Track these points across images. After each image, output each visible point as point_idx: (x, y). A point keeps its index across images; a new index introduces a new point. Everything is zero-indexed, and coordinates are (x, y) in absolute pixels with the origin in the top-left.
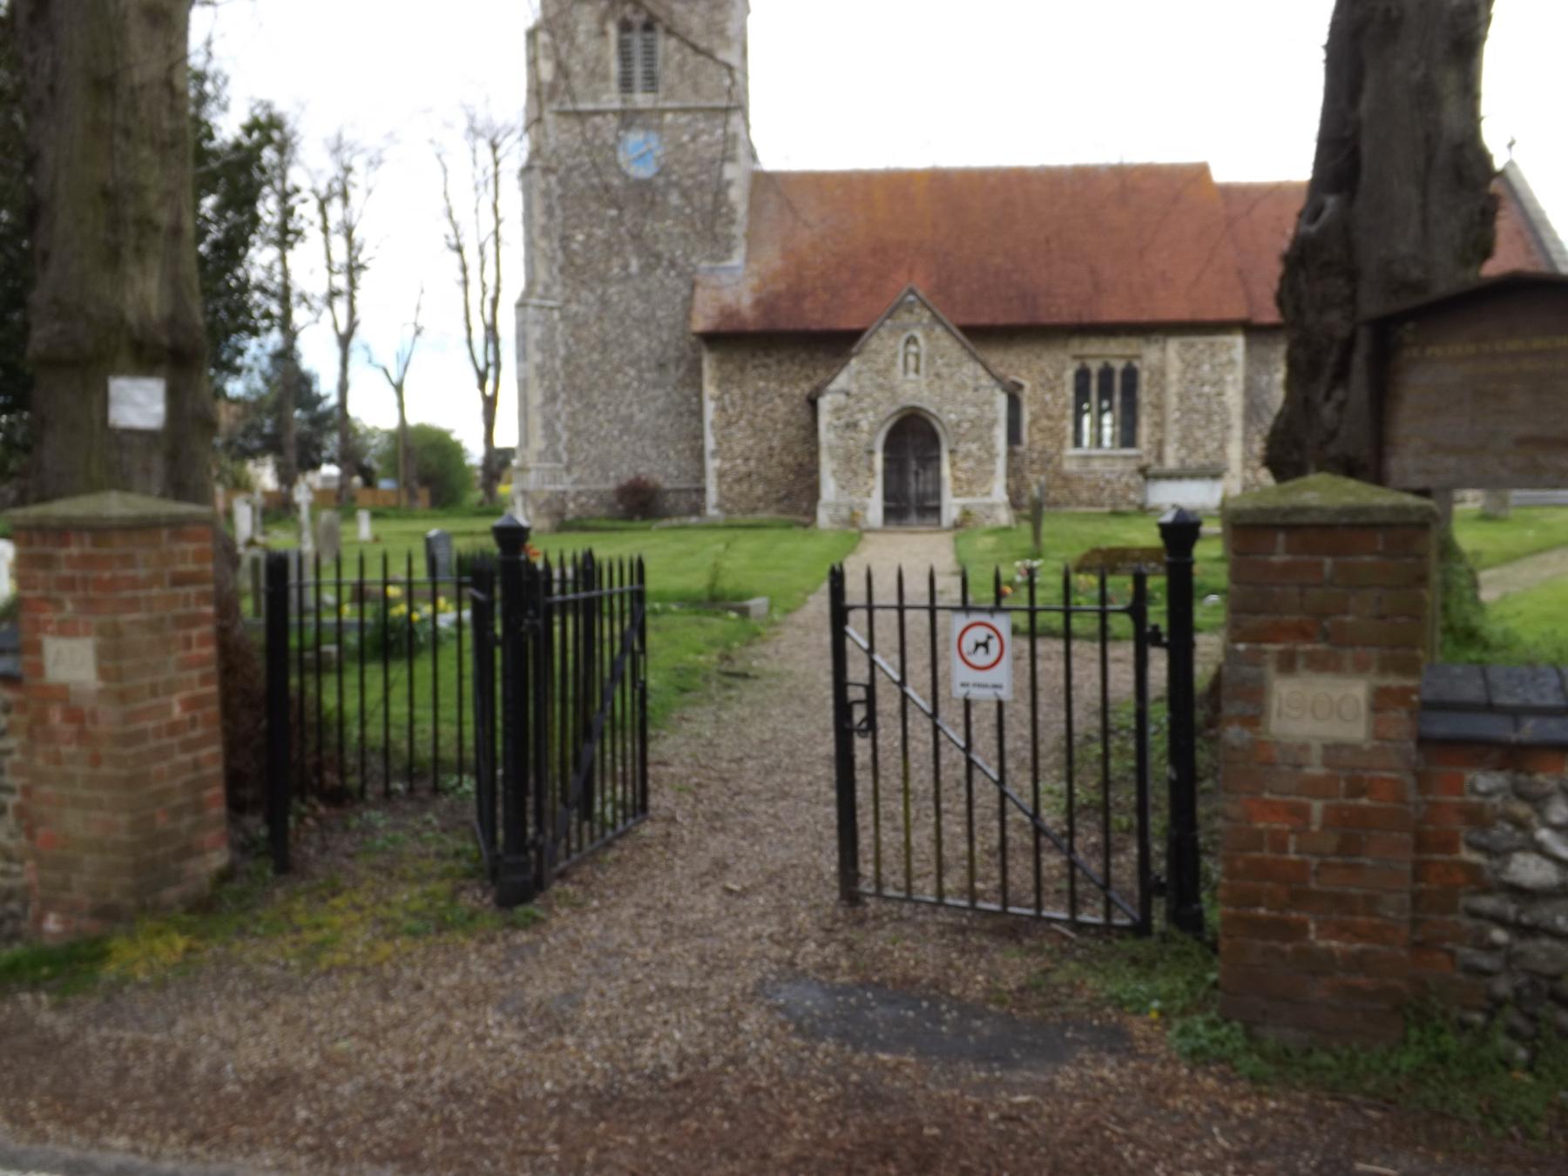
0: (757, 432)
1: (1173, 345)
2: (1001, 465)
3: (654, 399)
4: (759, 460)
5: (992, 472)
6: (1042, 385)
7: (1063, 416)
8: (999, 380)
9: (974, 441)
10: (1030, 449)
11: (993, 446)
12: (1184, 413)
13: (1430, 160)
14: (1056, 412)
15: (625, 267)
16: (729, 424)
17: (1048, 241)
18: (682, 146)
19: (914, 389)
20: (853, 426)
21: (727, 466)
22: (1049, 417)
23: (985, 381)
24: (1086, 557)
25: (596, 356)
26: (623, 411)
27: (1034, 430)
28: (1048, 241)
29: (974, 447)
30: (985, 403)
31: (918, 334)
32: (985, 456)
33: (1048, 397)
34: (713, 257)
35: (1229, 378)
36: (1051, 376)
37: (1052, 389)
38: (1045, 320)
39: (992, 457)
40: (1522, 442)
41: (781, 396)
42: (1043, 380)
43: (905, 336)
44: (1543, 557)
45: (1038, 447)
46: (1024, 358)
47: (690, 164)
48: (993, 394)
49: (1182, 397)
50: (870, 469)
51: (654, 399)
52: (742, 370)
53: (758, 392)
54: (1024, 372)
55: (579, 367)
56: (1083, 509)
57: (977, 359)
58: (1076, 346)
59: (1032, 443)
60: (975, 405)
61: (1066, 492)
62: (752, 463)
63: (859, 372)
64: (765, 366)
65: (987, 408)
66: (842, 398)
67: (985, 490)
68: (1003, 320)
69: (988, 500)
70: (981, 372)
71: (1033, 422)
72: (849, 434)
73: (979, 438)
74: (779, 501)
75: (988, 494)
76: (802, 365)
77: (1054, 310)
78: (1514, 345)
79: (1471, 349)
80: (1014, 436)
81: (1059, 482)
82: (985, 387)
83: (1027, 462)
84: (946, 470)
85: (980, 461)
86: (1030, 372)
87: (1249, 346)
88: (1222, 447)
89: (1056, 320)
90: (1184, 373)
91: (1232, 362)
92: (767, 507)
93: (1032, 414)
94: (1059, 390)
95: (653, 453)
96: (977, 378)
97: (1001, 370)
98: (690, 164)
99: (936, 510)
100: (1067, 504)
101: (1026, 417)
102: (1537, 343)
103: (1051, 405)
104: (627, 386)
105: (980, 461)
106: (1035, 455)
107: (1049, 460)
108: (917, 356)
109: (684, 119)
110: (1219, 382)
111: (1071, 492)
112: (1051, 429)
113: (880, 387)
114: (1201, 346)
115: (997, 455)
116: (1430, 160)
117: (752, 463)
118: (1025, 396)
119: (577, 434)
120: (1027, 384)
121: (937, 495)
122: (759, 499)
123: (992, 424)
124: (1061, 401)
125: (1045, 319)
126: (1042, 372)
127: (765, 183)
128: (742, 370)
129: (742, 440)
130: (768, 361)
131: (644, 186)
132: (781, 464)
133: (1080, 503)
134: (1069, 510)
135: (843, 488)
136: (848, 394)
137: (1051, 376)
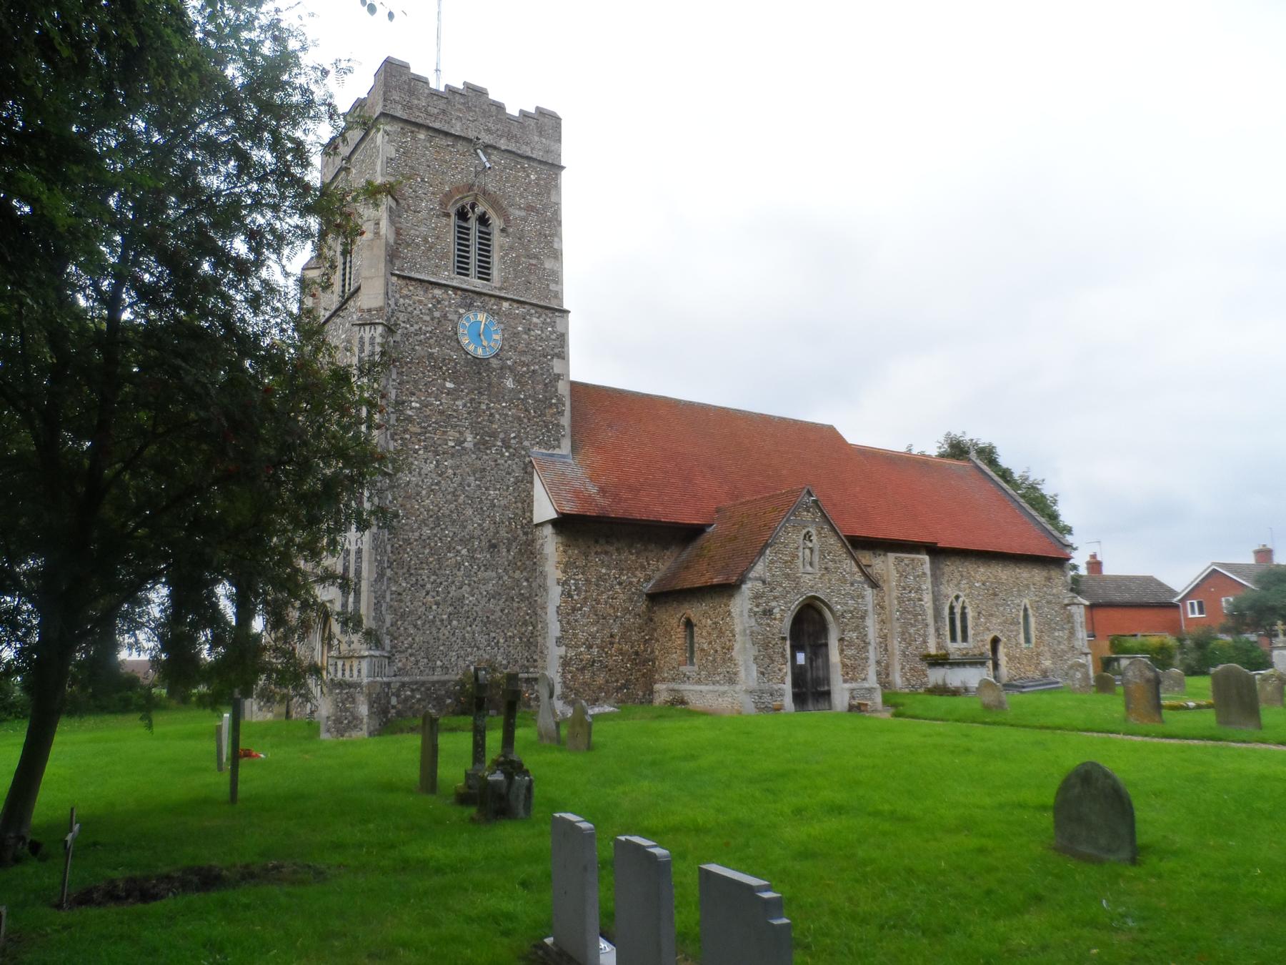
0: (601, 618)
1: (891, 557)
3: (486, 581)
4: (601, 648)
5: (867, 658)
9: (854, 631)
12: (902, 613)
15: (460, 442)
16: (574, 610)
18: (516, 334)
19: (812, 581)
20: (768, 613)
21: (571, 653)
25: (426, 531)
26: (453, 592)
31: (813, 532)
34: (548, 445)
35: (924, 587)
41: (620, 584)
43: (804, 531)
47: (523, 353)
49: (900, 600)
50: (783, 656)
51: (486, 581)
52: (586, 555)
53: (601, 578)
55: (408, 542)
62: (595, 650)
63: (772, 562)
64: (606, 553)
66: (759, 584)
72: (765, 621)
73: (856, 628)
74: (618, 689)
76: (638, 554)
84: (835, 656)
87: (932, 562)
88: (925, 642)
90: (899, 581)
91: (924, 574)
92: (608, 696)
95: (482, 640)
98: (523, 353)
99: (827, 694)
104: (458, 566)
108: (811, 550)
109: (520, 311)
110: (919, 590)
113: (787, 576)
114: (906, 561)
117: (595, 650)
119: (403, 616)
121: (827, 680)
122: (600, 689)
127: (579, 390)
128: (586, 555)
129: (586, 627)
130: (611, 549)
131: (478, 364)
132: (621, 652)
135: (763, 674)
136: (764, 582)
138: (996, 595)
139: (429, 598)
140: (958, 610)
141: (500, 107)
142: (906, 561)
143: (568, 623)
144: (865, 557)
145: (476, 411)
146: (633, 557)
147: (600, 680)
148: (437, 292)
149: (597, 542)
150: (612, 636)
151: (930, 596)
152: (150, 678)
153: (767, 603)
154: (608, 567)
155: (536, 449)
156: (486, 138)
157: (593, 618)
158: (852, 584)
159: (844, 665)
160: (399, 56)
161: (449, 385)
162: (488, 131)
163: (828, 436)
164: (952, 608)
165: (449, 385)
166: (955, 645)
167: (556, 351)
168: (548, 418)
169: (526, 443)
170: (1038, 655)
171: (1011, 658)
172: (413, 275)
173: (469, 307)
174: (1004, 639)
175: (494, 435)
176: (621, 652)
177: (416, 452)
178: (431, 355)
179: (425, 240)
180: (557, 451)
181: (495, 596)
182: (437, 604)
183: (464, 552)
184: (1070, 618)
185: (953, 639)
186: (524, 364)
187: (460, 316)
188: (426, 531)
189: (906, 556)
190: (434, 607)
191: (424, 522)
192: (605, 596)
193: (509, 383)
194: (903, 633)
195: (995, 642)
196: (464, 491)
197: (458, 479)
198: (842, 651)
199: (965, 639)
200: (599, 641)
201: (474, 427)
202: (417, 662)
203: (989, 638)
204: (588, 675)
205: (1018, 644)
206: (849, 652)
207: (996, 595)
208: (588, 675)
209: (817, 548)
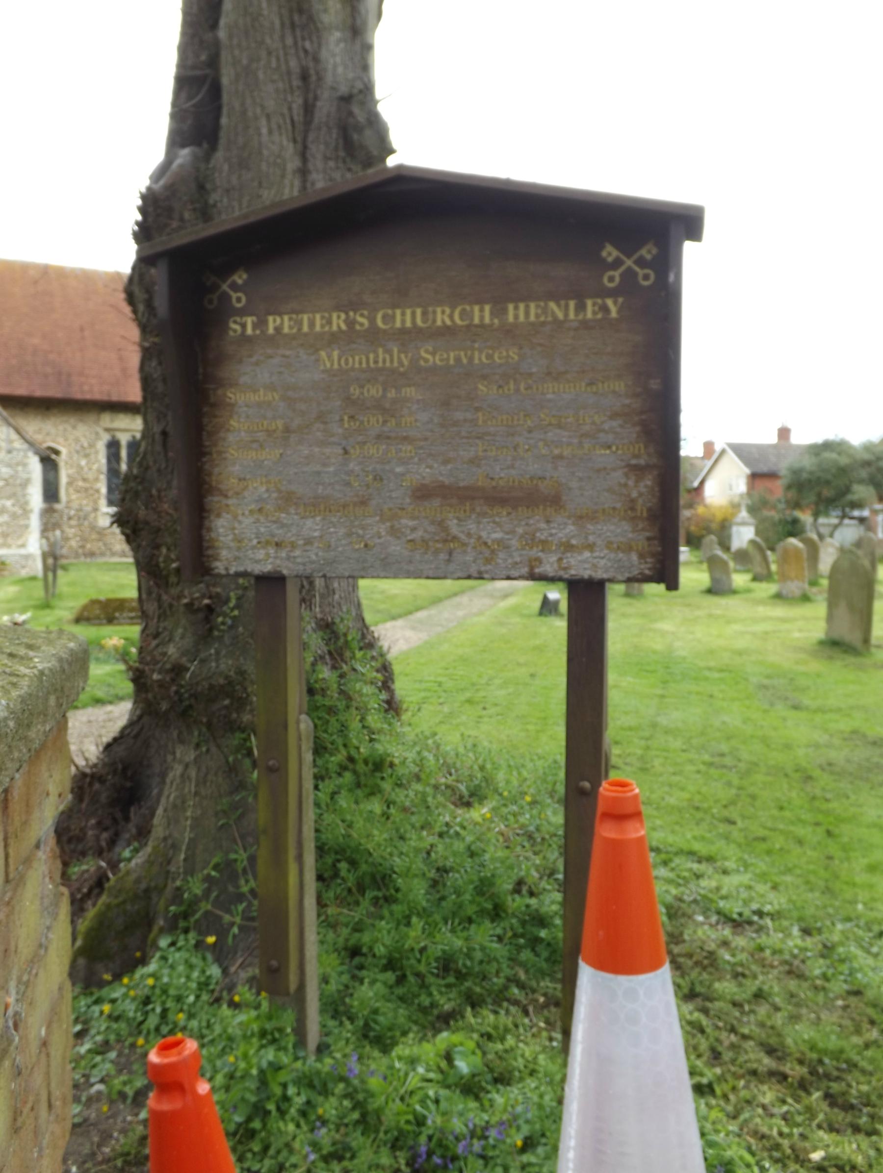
2: (35, 522)
5: (27, 527)
6: (78, 452)
7: (97, 480)
8: (31, 444)
9: (9, 498)
10: (67, 507)
11: (27, 503)
13: (308, 109)
14: (91, 476)
17: (82, 329)
22: (85, 480)
23: (18, 444)
24: (85, 608)
27: (71, 490)
28: (82, 329)
29: (9, 503)
30: (18, 464)
32: (20, 512)
33: (83, 462)
36: (86, 445)
37: (86, 456)
38: (79, 396)
39: (26, 512)
40: (423, 493)
42: (78, 448)
44: (457, 599)
45: (75, 505)
46: (61, 428)
48: (26, 456)
54: (61, 440)
56: (116, 559)
57: (9, 424)
58: (107, 420)
59: (68, 502)
60: (9, 465)
61: (101, 544)
65: (20, 468)
67: (20, 542)
68: (39, 393)
69: (23, 551)
70: (14, 436)
71: (70, 484)
73: (13, 495)
75: (23, 546)
77: (86, 388)
78: (406, 318)
79: (338, 322)
80: (51, 493)
81: (94, 536)
82: (18, 450)
83: (65, 519)
85: (14, 516)
86: (66, 440)
89: (88, 397)
93: (69, 476)
94: (92, 457)
96: (10, 442)
97: (38, 437)
100: (102, 554)
101: (64, 479)
102: (442, 316)
103: (86, 469)
105: (14, 516)
106: (72, 513)
107: (85, 518)
111: (105, 545)
112: (86, 490)
115: (31, 511)
116: (308, 109)
118: (62, 460)
120: (64, 451)
123: (26, 483)
124: (95, 467)
125: (77, 394)
126: (77, 440)
133: (113, 554)
134: (101, 560)
137: (86, 445)
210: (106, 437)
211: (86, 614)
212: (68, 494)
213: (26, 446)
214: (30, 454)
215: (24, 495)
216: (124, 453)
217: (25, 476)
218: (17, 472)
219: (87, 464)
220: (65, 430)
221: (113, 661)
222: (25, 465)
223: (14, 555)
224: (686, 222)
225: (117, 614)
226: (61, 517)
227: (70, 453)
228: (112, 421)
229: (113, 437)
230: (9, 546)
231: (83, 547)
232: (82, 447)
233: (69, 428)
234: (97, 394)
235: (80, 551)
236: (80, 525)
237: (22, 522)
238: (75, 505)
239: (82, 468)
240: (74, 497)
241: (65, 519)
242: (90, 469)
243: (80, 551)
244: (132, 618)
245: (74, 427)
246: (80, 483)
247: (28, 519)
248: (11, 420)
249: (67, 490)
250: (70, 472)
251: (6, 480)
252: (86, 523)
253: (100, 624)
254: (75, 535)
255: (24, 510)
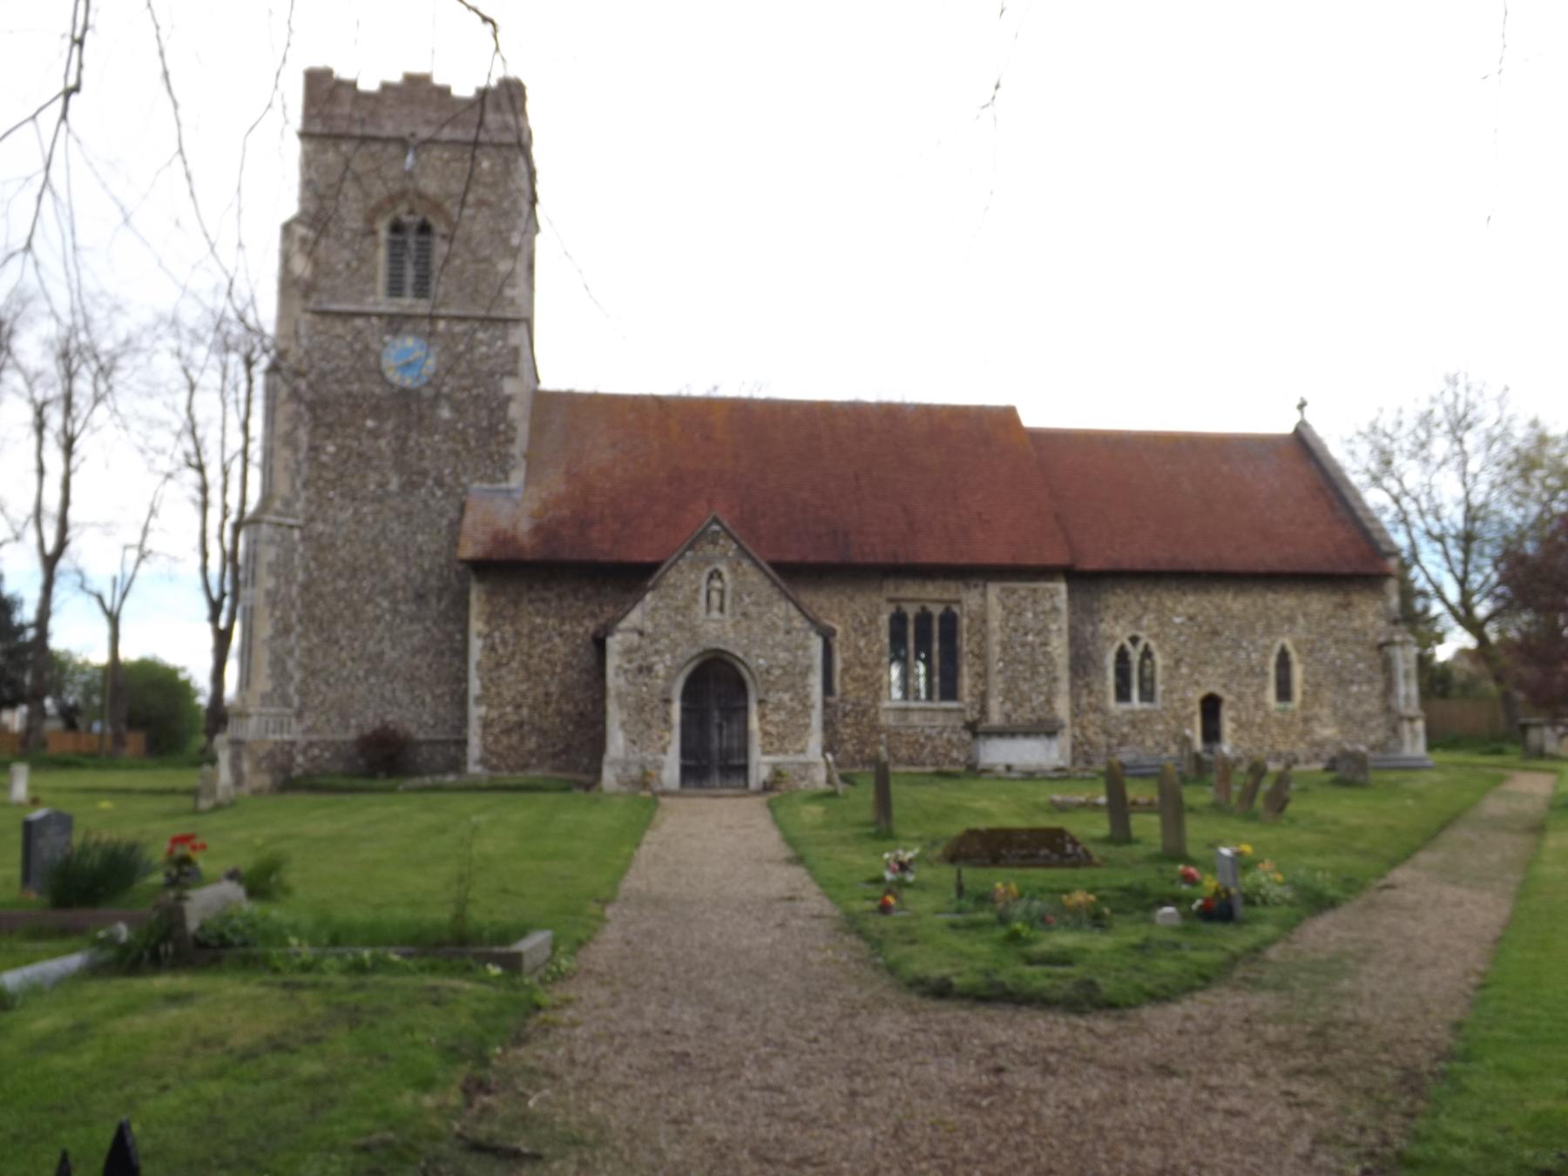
0: (530, 674)
1: (994, 590)
3: (410, 635)
5: (807, 726)
6: (855, 630)
9: (786, 690)
10: (842, 701)
11: (807, 696)
14: (870, 660)
15: (382, 485)
16: (498, 665)
17: (857, 478)
19: (717, 629)
20: (648, 670)
21: (494, 714)
22: (863, 665)
23: (799, 622)
25: (341, 584)
26: (372, 647)
27: (847, 679)
29: (786, 697)
30: (797, 648)
31: (723, 568)
32: (799, 708)
35: (1054, 627)
36: (865, 620)
37: (865, 634)
38: (858, 559)
39: (807, 708)
41: (561, 635)
43: (708, 570)
45: (851, 697)
46: (836, 600)
47: (463, 376)
48: (807, 637)
49: (1005, 647)
52: (516, 604)
54: (836, 616)
55: (320, 596)
57: (789, 598)
58: (890, 588)
59: (843, 694)
60: (787, 649)
62: (525, 711)
63: (655, 609)
64: (543, 600)
65: (800, 653)
66: (635, 638)
67: (798, 747)
68: (812, 558)
69: (801, 758)
70: (794, 612)
71: (845, 670)
73: (792, 687)
74: (555, 756)
75: (802, 751)
82: (798, 630)
83: (840, 714)
84: (754, 723)
85: (792, 713)
86: (842, 615)
87: (1070, 592)
88: (1049, 702)
90: (1006, 620)
91: (1055, 609)
93: (844, 661)
94: (873, 635)
95: (404, 698)
98: (463, 376)
99: (744, 769)
103: (865, 652)
104: (378, 619)
105: (792, 713)
109: (459, 328)
110: (1043, 631)
112: (865, 678)
113: (679, 626)
115: (812, 707)
117: (525, 711)
119: (314, 673)
121: (744, 751)
122: (531, 753)
124: (876, 648)
126: (855, 615)
128: (516, 604)
129: (513, 684)
130: (547, 594)
131: (405, 397)
135: (634, 742)
136: (641, 633)
137: (865, 620)
138: (1215, 633)
139: (344, 655)
140: (1135, 656)
141: (444, 92)
142: (1023, 593)
143: (491, 680)
144: (822, 601)
145: (401, 450)
146: (580, 604)
147: (532, 743)
148: (359, 322)
149: (531, 588)
150: (547, 694)
151: (1065, 638)
152: (842, 730)
153: (644, 658)
154: (545, 616)
155: (476, 485)
156: (425, 133)
157: (522, 674)
158: (788, 632)
159: (766, 734)
160: (319, 63)
161: (370, 423)
162: (428, 122)
163: (1007, 416)
164: (1122, 656)
165: (370, 423)
166: (1124, 706)
167: (508, 368)
168: (493, 448)
169: (464, 479)
170: (1306, 720)
171: (1241, 725)
172: (335, 307)
173: (396, 332)
174: (1228, 698)
175: (424, 473)
176: (559, 712)
177: (331, 500)
178: (349, 394)
179: (348, 265)
180: (503, 485)
181: (423, 650)
182: (353, 660)
183: (385, 604)
184: (1387, 666)
185: (1123, 694)
186: (464, 389)
187: (385, 345)
188: (341, 584)
189: (1023, 588)
190: (349, 664)
191: (339, 575)
192: (539, 650)
193: (445, 413)
194: (1009, 691)
195: (1211, 706)
196: (385, 538)
197: (379, 526)
198: (762, 717)
199: (1147, 695)
200: (530, 701)
201: (400, 467)
202: (328, 721)
203: (1196, 696)
204: (515, 738)
205: (1260, 705)
206: (775, 717)
207: (1215, 633)
208: (515, 738)
209: (729, 589)
210: (892, 608)
211: (963, 850)
212: (843, 684)
213: (807, 624)
214: (812, 634)
215: (804, 687)
216: (911, 630)
217: (806, 662)
218: (796, 657)
219: (867, 644)
220: (841, 603)
221: (1087, 927)
222: (806, 648)
223: (792, 763)
224: (323, 90)
225: (1004, 852)
226: (835, 713)
227: (846, 631)
228: (897, 589)
229: (898, 609)
230: (786, 752)
231: (861, 752)
232: (861, 622)
233: (846, 601)
234: (881, 556)
235: (858, 757)
236: (857, 724)
237: (801, 721)
238: (851, 697)
239: (860, 650)
240: (850, 687)
241: (840, 714)
242: (870, 651)
243: (858, 757)
244: (1023, 857)
245: (851, 599)
246: (859, 671)
247: (809, 716)
248: (791, 593)
249: (842, 679)
250: (846, 655)
251: (783, 668)
252: (865, 720)
253: (984, 865)
254: (851, 737)
255: (804, 705)
